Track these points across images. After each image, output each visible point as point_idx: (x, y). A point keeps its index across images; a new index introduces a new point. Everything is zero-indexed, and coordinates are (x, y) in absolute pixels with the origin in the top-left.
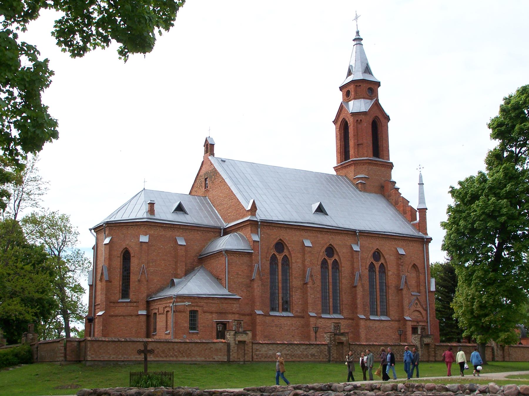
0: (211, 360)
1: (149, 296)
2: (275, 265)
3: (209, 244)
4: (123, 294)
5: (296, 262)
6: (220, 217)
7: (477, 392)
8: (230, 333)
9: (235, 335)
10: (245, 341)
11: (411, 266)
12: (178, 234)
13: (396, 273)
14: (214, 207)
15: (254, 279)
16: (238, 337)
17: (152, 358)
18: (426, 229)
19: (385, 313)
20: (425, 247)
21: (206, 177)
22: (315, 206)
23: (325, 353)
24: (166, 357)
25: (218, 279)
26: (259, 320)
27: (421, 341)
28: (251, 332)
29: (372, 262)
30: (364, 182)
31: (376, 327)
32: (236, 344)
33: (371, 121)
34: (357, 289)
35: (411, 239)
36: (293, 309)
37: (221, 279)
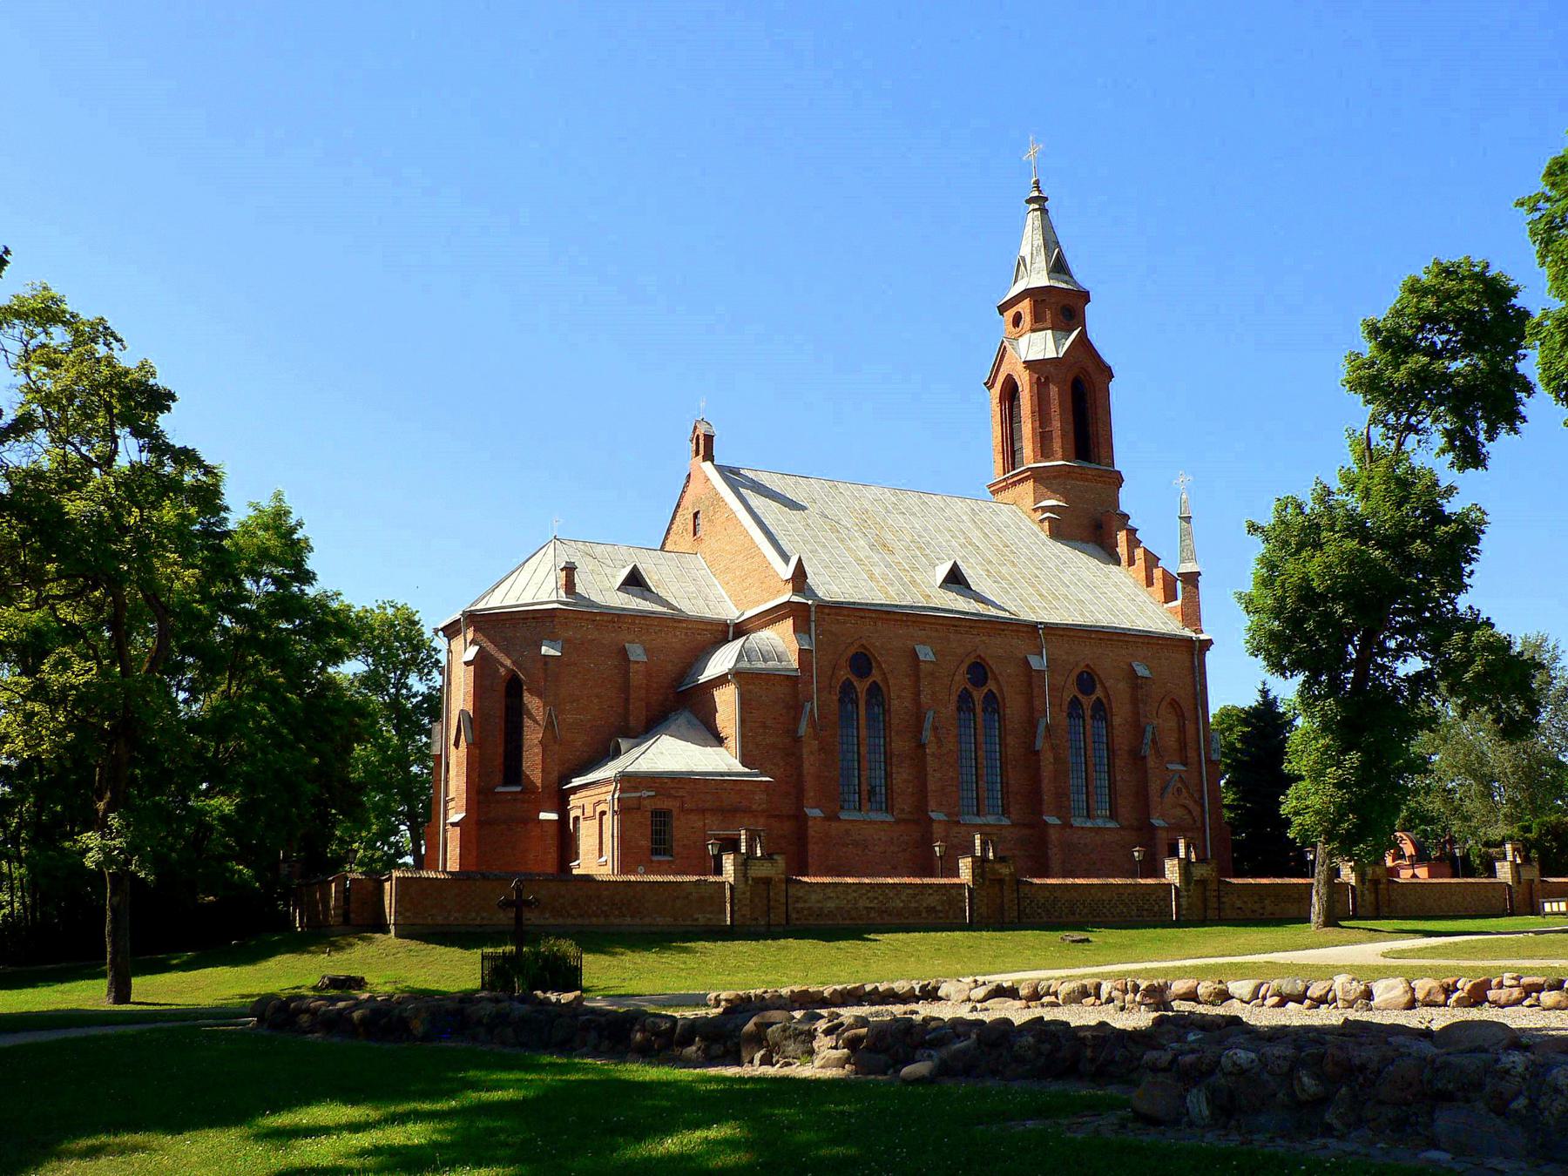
5: (899, 697)
12: (630, 637)
13: (1129, 719)
19: (889, 809)
22: (943, 571)
24: (581, 916)
26: (812, 831)
29: (1075, 697)
31: (1085, 844)
33: (1070, 377)
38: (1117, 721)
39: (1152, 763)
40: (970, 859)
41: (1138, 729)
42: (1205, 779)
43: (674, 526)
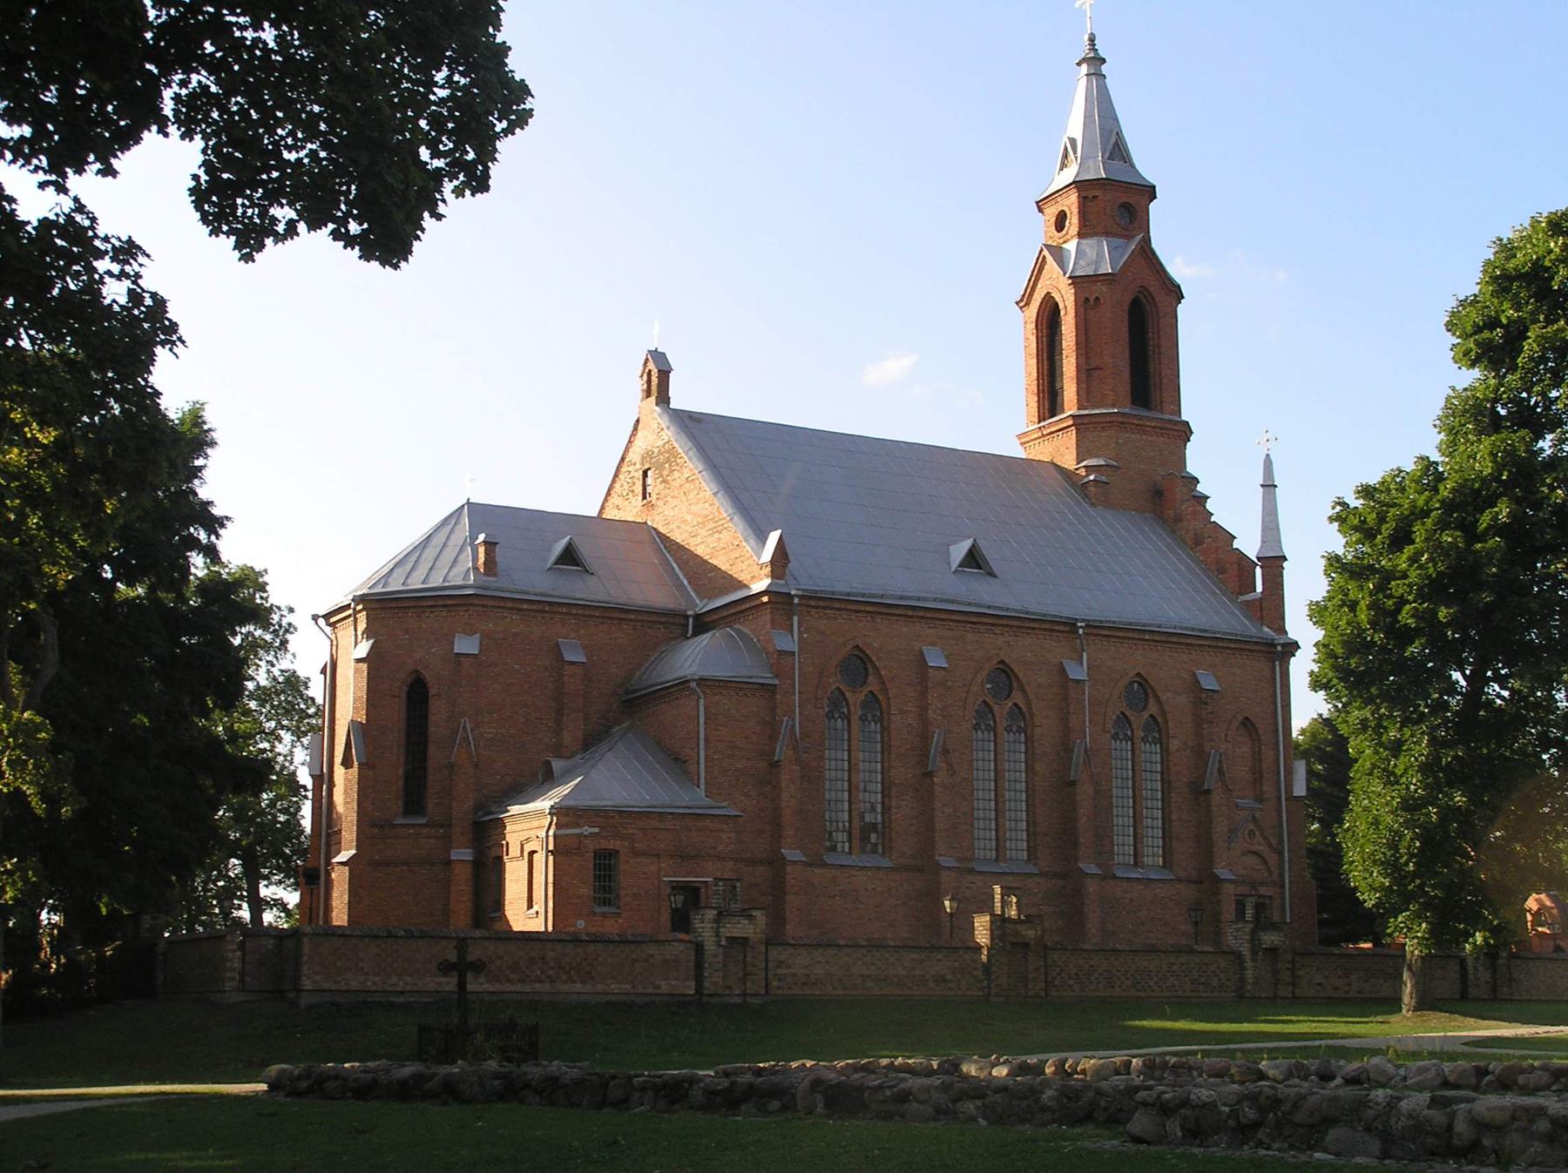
0: (650, 991)
1: (480, 807)
2: (843, 720)
3: (652, 659)
4: (406, 803)
6: (686, 582)
7: (1338, 1081)
8: (703, 915)
9: (718, 919)
10: (746, 939)
11: (1235, 724)
14: (669, 552)
15: (779, 761)
16: (728, 925)
17: (482, 984)
18: (1283, 618)
20: (1278, 668)
21: (646, 467)
22: (960, 550)
23: (976, 973)
24: (522, 981)
25: (678, 762)
27: (1254, 942)
28: (764, 912)
30: (1104, 479)
31: (1131, 900)
32: (720, 946)
34: (1078, 791)
35: (1237, 646)
36: (891, 848)
37: (685, 762)
38: (1174, 745)
39: (1217, 798)
40: (988, 918)
41: (1201, 755)
42: (1284, 819)
43: (617, 485)
